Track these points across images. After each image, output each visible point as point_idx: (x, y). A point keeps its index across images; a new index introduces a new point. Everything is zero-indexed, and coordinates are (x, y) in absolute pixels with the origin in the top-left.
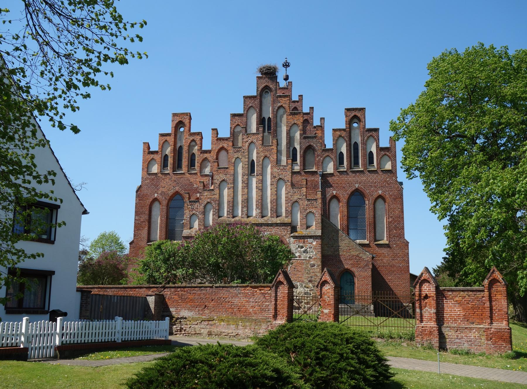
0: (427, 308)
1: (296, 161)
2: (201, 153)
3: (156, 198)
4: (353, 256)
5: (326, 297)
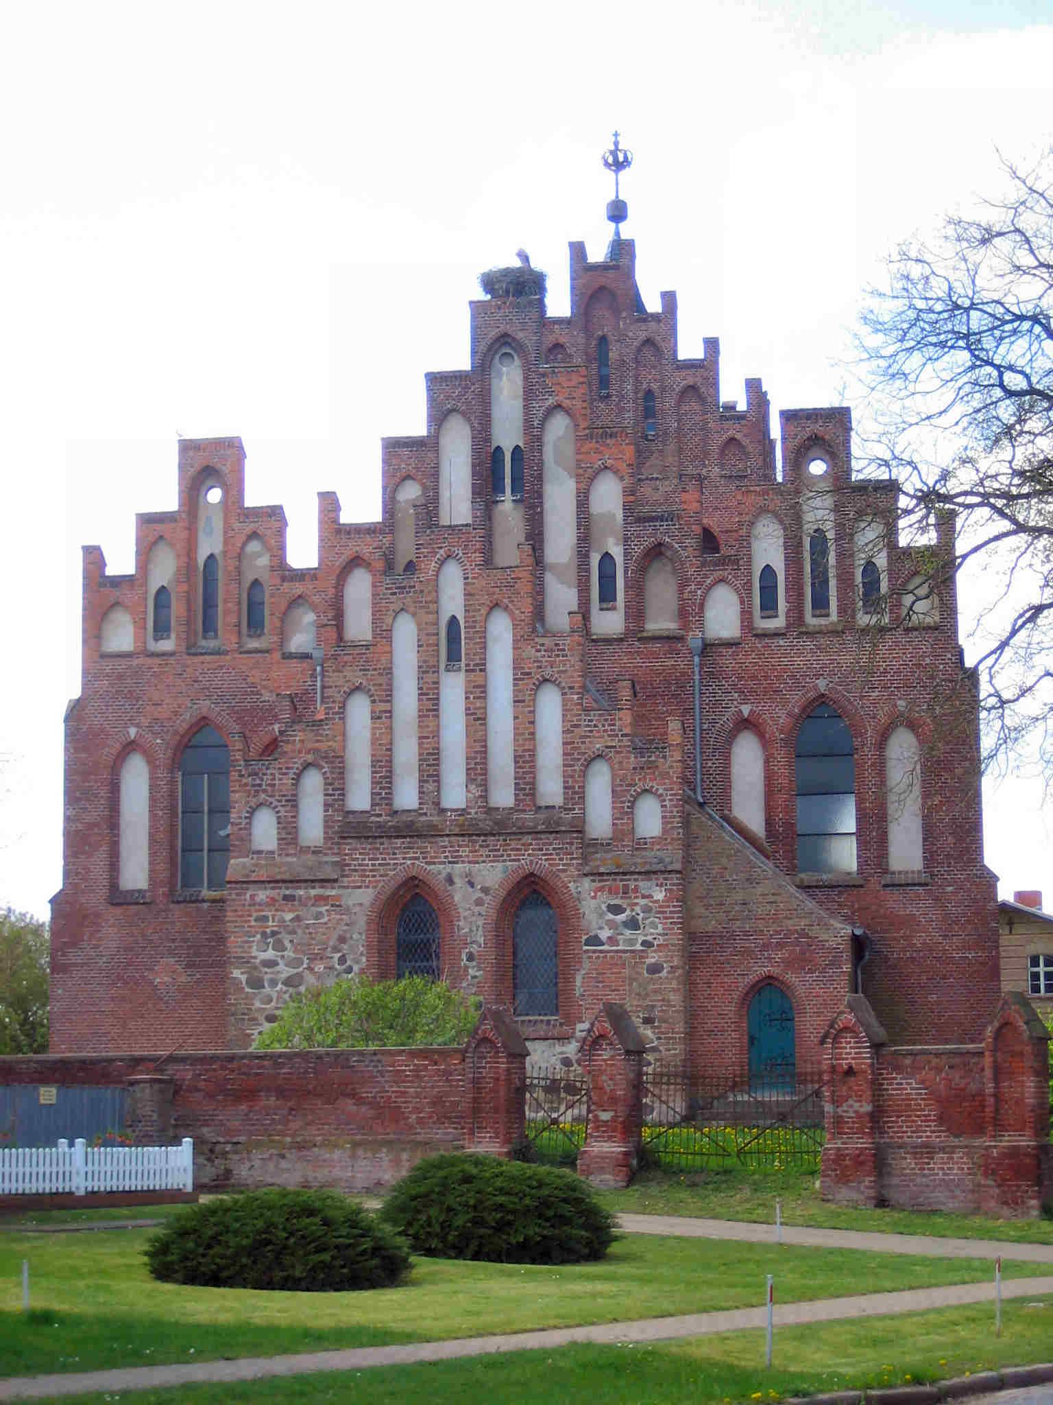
0: (850, 1102)
1: (615, 600)
2: (283, 579)
3: (133, 742)
4: (791, 932)
5: (604, 1078)
